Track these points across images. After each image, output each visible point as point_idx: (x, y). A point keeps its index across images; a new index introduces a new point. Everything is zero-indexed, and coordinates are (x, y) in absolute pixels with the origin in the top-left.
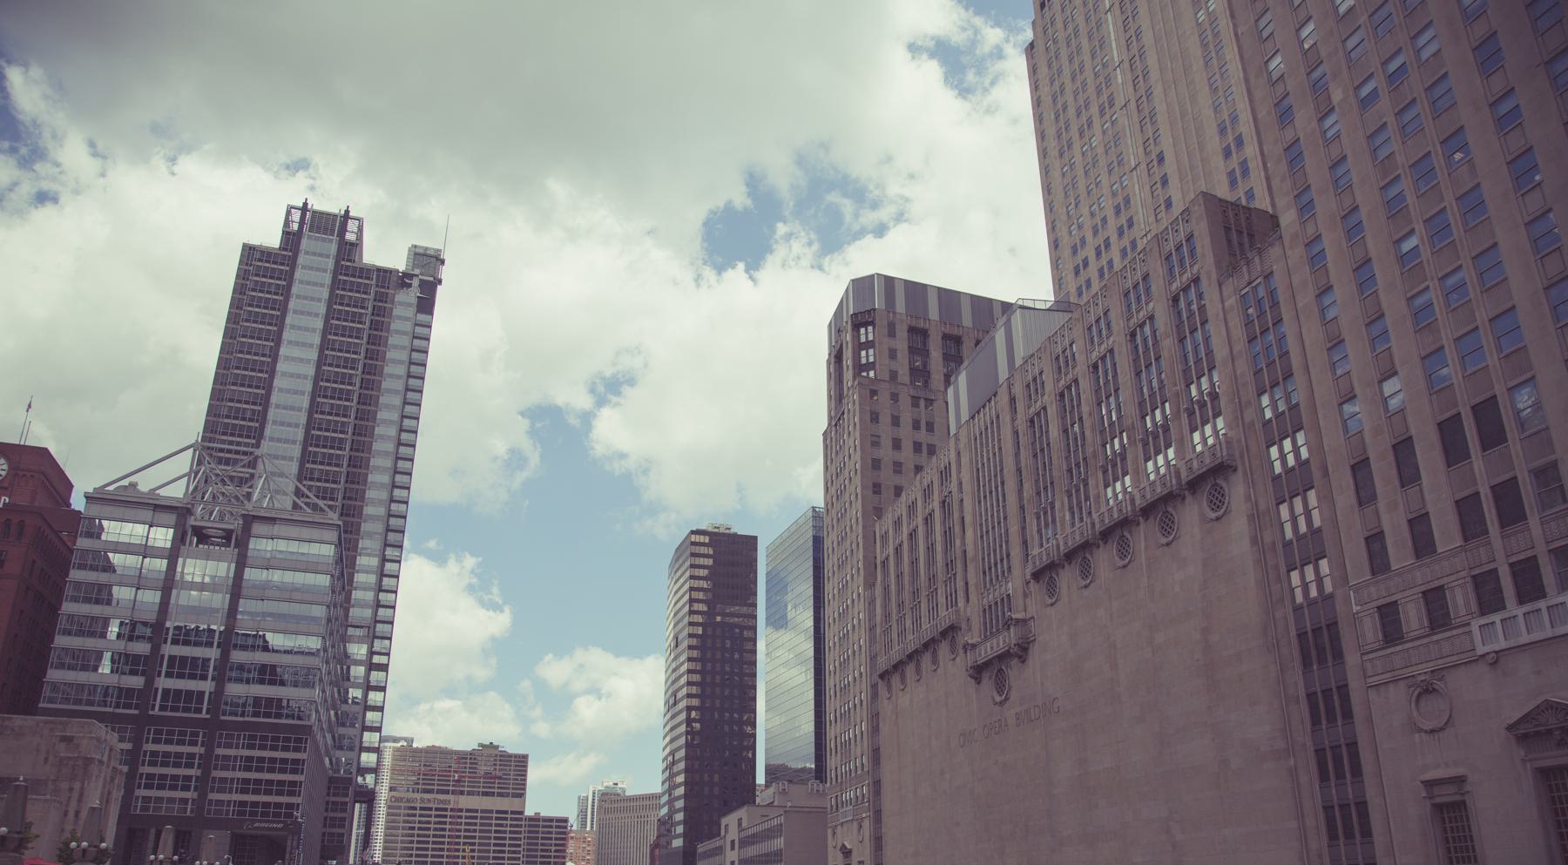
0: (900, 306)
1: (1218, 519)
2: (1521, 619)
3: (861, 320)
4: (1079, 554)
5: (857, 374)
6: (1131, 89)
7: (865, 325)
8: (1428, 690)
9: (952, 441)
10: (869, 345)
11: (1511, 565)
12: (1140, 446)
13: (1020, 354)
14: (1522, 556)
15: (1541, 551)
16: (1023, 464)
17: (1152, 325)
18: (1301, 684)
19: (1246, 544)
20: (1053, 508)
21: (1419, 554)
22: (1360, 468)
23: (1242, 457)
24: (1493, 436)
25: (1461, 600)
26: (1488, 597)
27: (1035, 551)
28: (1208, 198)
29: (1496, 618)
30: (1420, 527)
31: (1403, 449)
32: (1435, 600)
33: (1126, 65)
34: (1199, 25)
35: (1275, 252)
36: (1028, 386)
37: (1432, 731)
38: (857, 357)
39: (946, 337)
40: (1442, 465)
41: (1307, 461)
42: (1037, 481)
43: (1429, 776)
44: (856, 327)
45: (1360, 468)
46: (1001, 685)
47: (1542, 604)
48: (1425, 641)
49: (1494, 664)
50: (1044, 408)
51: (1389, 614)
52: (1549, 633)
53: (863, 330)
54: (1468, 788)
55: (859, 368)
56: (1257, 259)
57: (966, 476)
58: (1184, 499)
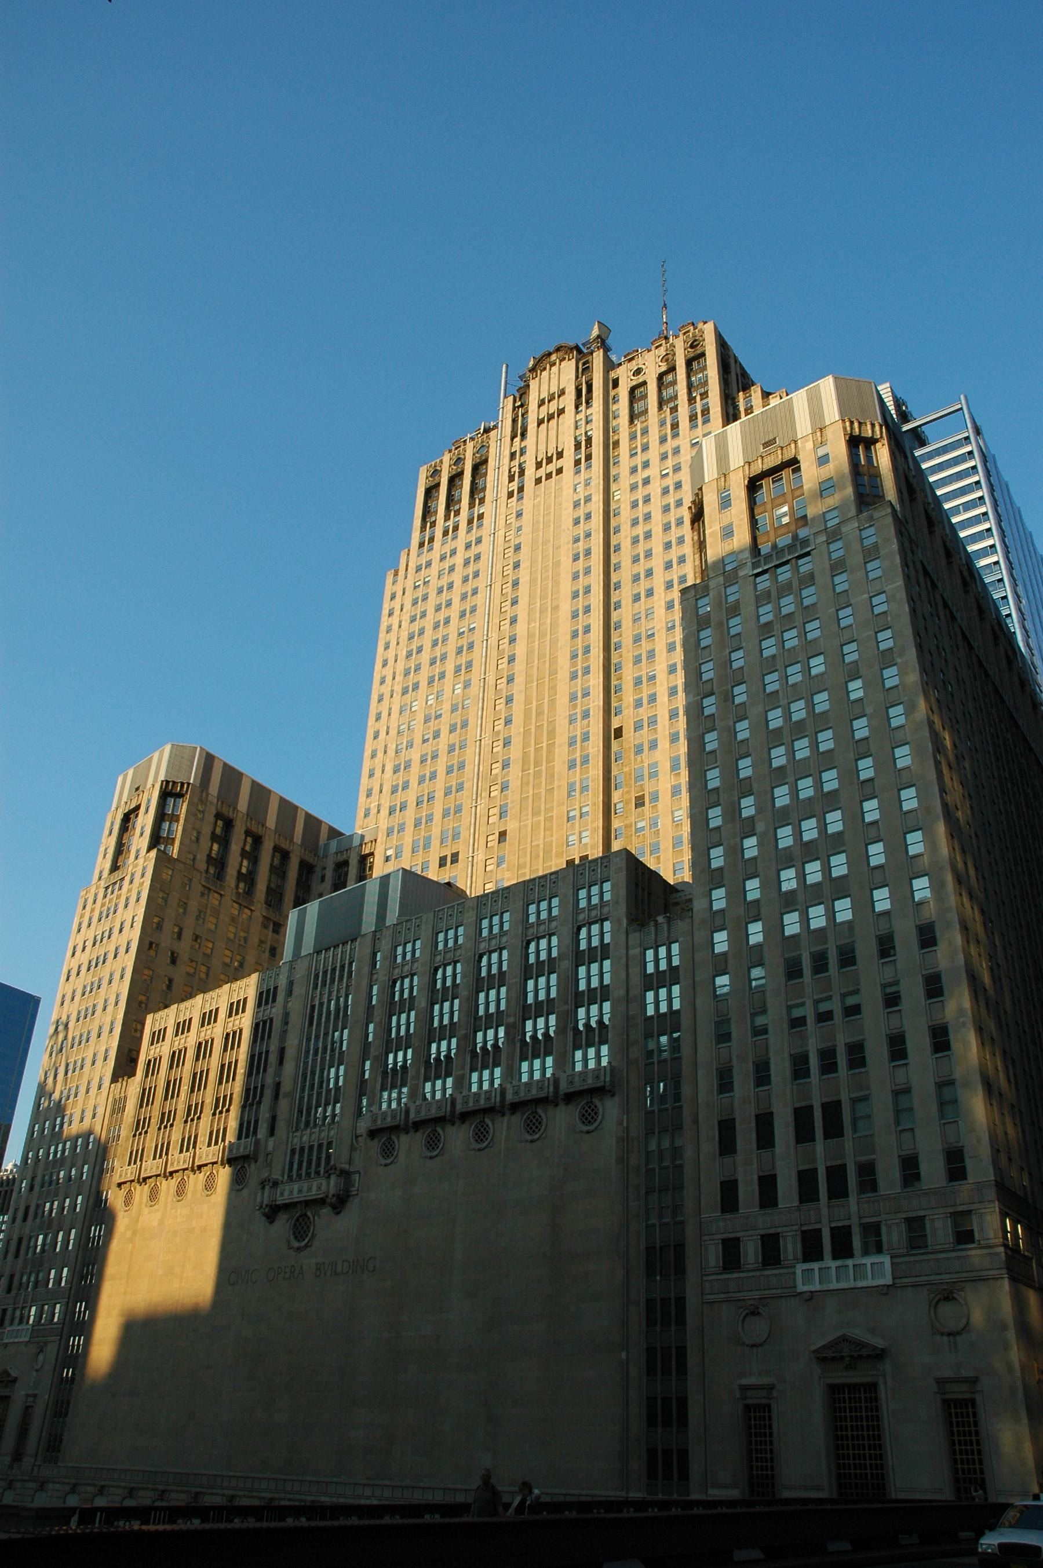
0: (214, 788)
2: (869, 1266)
14: (840, 1224)
15: (854, 1222)
21: (763, 1205)
25: (791, 1247)
26: (811, 1250)
29: (816, 1266)
30: (768, 1184)
34: (648, 1153)
37: (753, 1346)
40: (792, 1140)
41: (678, 1012)
46: (302, 1230)
47: (850, 1262)
52: (851, 1284)
54: (775, 1394)
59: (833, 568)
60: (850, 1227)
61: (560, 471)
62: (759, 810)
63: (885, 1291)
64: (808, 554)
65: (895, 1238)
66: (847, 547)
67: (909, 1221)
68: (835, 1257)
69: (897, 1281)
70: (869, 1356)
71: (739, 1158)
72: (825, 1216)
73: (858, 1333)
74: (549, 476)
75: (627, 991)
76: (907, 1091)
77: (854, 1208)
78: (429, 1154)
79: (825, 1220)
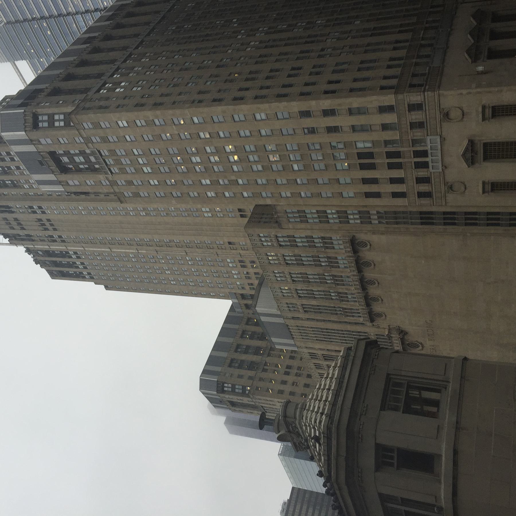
0: (218, 369)
1: (370, 245)
3: (220, 388)
4: (368, 301)
5: (248, 396)
6: (151, 248)
7: (223, 387)
8: (451, 188)
9: (300, 350)
10: (233, 387)
11: (414, 157)
12: (332, 269)
13: (275, 311)
16: (323, 318)
17: (286, 256)
18: (440, 227)
19: (383, 238)
20: (345, 309)
22: (368, 195)
23: (350, 233)
24: (370, 155)
25: (422, 173)
27: (361, 320)
28: (246, 227)
31: (365, 181)
32: (420, 180)
33: (139, 247)
35: (278, 208)
36: (290, 310)
38: (238, 394)
39: (236, 351)
42: (331, 314)
43: (481, 191)
44: (223, 392)
45: (368, 195)
47: (429, 152)
48: (433, 185)
49: (446, 168)
50: (302, 305)
51: (421, 195)
53: (226, 389)
54: (487, 181)
55: (244, 393)
56: (279, 214)
57: (318, 346)
58: (359, 256)
59: (105, 142)
60: (415, 162)
61: (49, 220)
62: (226, 177)
63: (443, 140)
64: (99, 152)
65: (419, 134)
66: (95, 136)
67: (411, 128)
68: (427, 156)
69: (438, 134)
70: (471, 146)
71: (382, 191)
72: (409, 160)
73: (461, 150)
74: (52, 225)
75: (308, 229)
76: (353, 127)
77: (405, 149)
78: (373, 265)
79: (410, 160)
